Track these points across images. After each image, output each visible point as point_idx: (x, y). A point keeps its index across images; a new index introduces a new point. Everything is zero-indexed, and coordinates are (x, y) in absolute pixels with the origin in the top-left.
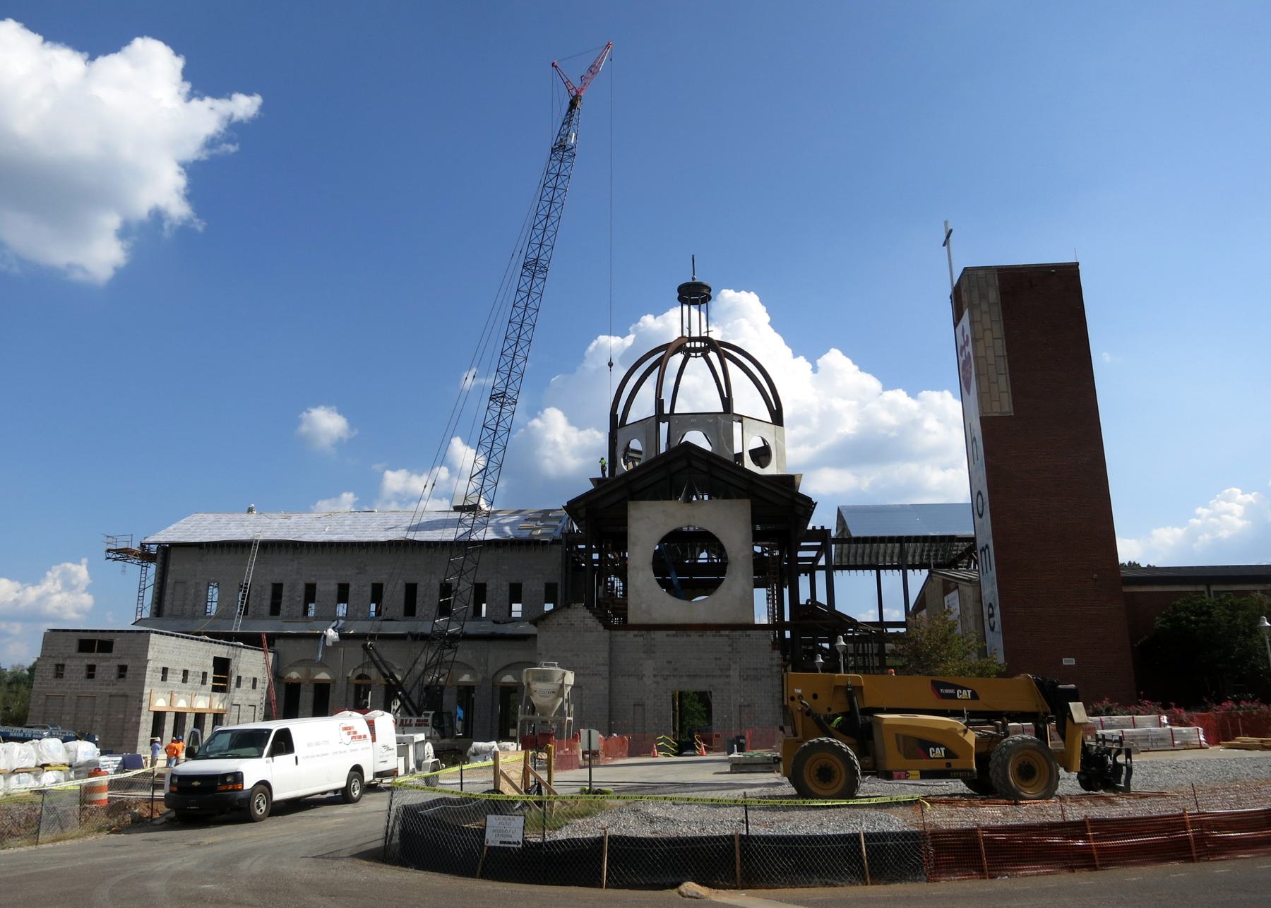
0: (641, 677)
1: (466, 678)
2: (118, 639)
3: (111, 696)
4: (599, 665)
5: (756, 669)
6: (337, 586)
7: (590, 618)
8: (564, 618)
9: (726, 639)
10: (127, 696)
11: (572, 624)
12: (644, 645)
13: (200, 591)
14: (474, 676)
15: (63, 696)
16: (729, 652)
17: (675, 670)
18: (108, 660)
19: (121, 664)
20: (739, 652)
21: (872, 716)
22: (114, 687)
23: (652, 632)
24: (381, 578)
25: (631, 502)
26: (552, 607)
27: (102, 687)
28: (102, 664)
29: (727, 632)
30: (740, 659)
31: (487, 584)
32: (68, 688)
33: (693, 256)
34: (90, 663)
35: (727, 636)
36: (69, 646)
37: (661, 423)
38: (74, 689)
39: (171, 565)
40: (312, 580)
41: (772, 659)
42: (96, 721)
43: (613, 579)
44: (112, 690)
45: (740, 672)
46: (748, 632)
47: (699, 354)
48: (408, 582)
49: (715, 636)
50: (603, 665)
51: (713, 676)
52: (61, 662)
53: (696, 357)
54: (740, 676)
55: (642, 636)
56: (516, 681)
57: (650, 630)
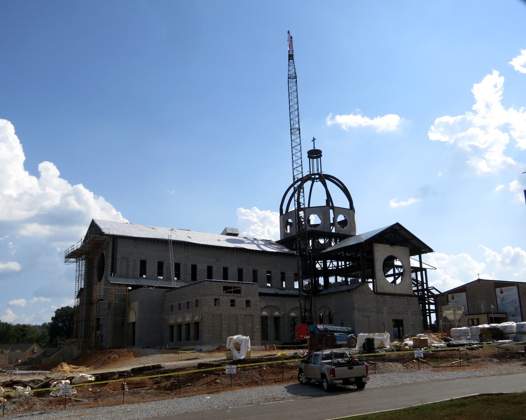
1: (277, 314)
2: (243, 287)
3: (245, 315)
6: (207, 267)
8: (361, 288)
10: (253, 316)
11: (364, 291)
13: (137, 264)
14: (280, 313)
15: (221, 315)
17: (393, 311)
18: (241, 297)
19: (247, 299)
21: (15, 351)
22: (246, 311)
23: (385, 296)
24: (227, 265)
25: (375, 244)
27: (239, 311)
28: (238, 299)
29: (406, 297)
31: (272, 271)
32: (223, 311)
33: (523, 173)
34: (232, 299)
35: (407, 299)
36: (220, 289)
37: (330, 210)
38: (226, 311)
39: (118, 248)
40: (195, 263)
42: (240, 328)
44: (245, 312)
46: (412, 298)
47: (318, 180)
48: (239, 268)
49: (403, 298)
52: (217, 298)
53: (317, 181)
54: (411, 314)
55: (382, 297)
56: (296, 315)
57: (384, 295)
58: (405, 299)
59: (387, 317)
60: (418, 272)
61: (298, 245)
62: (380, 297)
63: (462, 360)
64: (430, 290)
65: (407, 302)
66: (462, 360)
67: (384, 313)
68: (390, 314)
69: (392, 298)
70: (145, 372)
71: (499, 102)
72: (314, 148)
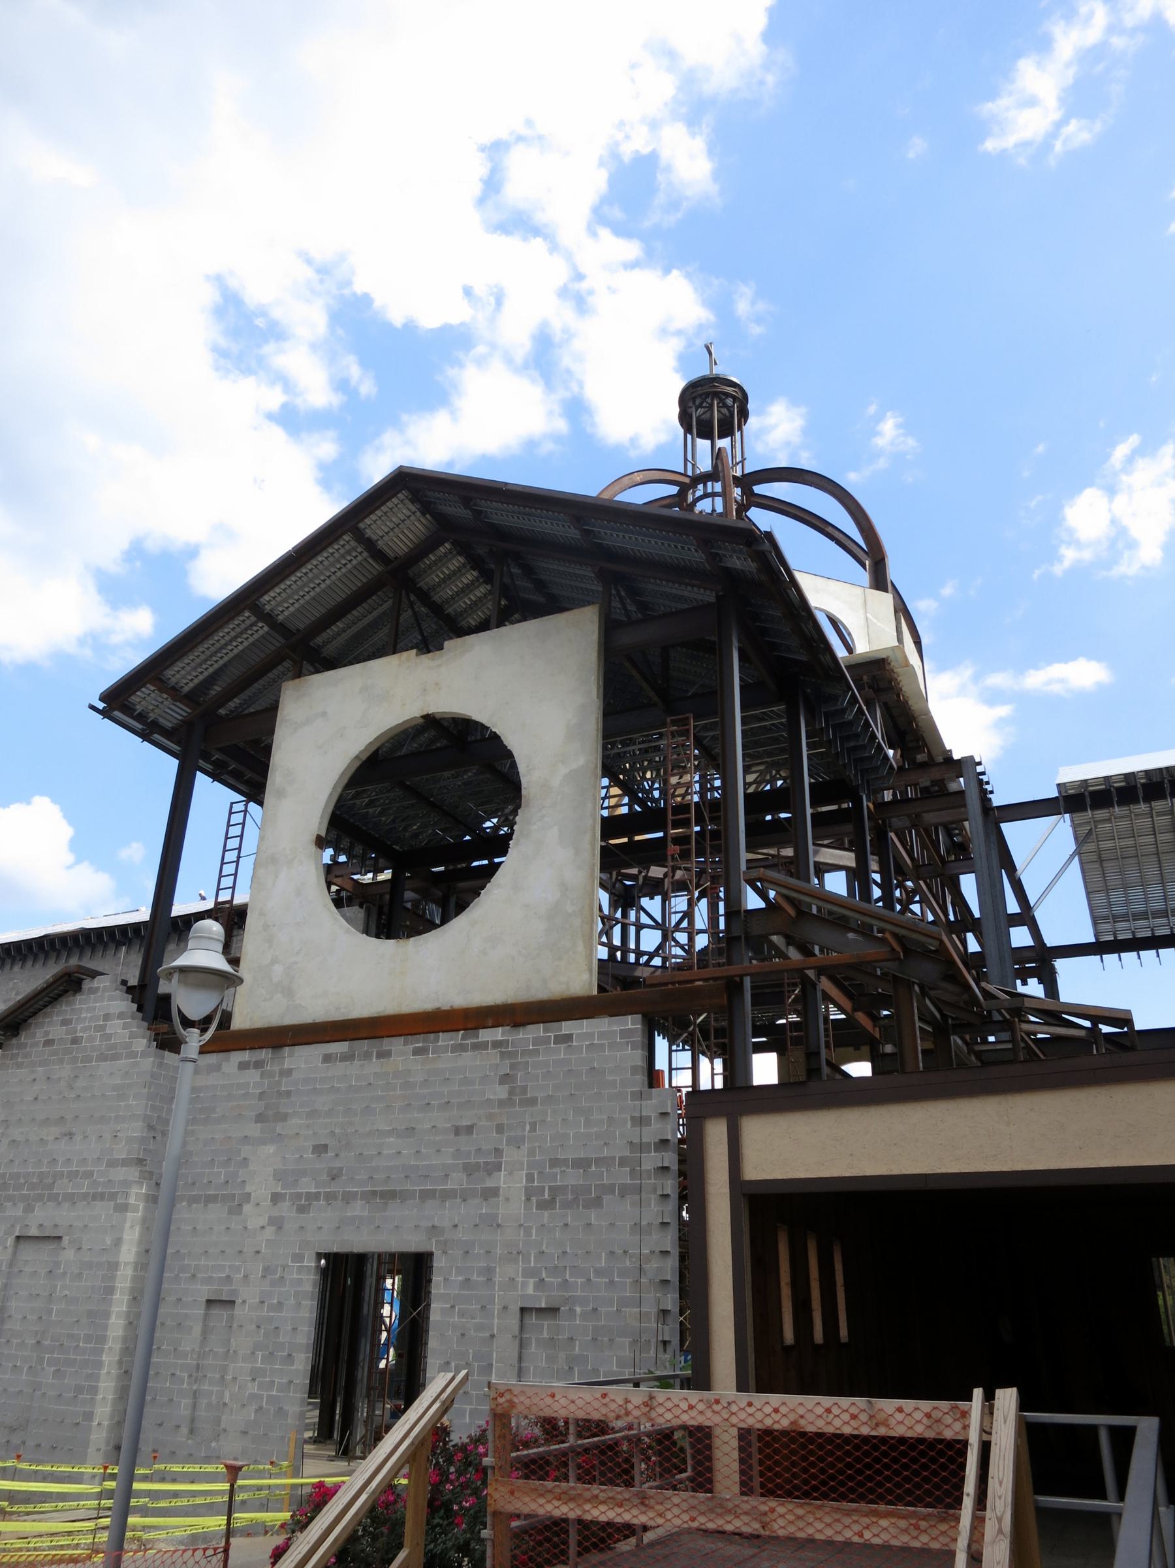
0: (237, 1204)
4: (112, 1164)
5: (580, 1163)
7: (121, 1016)
9: (493, 1055)
12: (262, 1095)
16: (501, 1103)
20: (533, 1101)
26: (971, 934)
29: (498, 1034)
30: (533, 1127)
35: (497, 1044)
41: (641, 1121)
43: (716, 795)
45: (530, 1178)
46: (566, 1027)
49: (461, 1048)
50: (125, 1163)
51: (447, 1195)
55: (258, 1065)
58: (483, 1046)
59: (270, 1232)
60: (999, 1393)
61: (395, 539)
62: (243, 1066)
63: (722, 926)
64: (806, 971)
65: (505, 1079)
66: (722, 926)
67: (247, 1197)
68: (302, 1210)
69: (347, 1057)
70: (157, 737)
71: (664, 332)
72: (1120, 957)
